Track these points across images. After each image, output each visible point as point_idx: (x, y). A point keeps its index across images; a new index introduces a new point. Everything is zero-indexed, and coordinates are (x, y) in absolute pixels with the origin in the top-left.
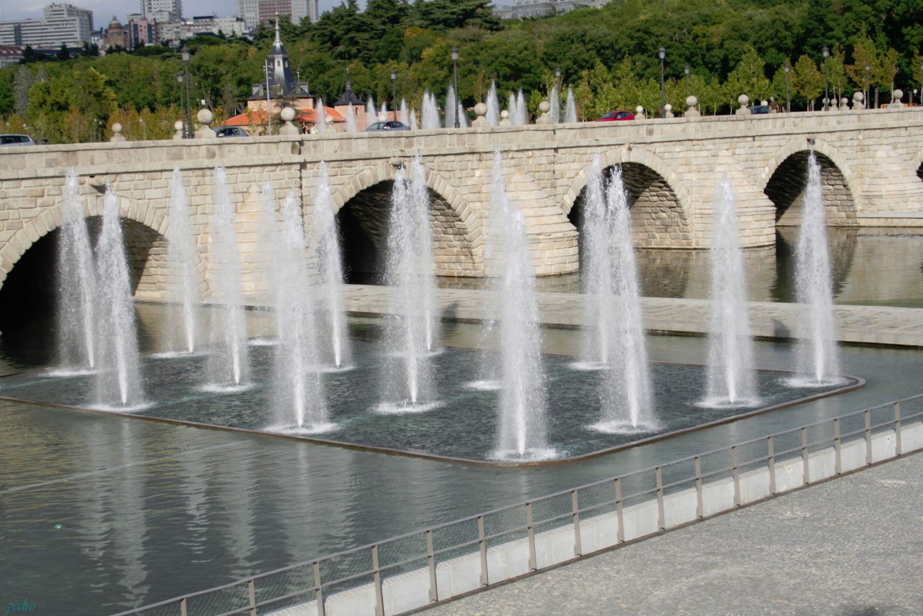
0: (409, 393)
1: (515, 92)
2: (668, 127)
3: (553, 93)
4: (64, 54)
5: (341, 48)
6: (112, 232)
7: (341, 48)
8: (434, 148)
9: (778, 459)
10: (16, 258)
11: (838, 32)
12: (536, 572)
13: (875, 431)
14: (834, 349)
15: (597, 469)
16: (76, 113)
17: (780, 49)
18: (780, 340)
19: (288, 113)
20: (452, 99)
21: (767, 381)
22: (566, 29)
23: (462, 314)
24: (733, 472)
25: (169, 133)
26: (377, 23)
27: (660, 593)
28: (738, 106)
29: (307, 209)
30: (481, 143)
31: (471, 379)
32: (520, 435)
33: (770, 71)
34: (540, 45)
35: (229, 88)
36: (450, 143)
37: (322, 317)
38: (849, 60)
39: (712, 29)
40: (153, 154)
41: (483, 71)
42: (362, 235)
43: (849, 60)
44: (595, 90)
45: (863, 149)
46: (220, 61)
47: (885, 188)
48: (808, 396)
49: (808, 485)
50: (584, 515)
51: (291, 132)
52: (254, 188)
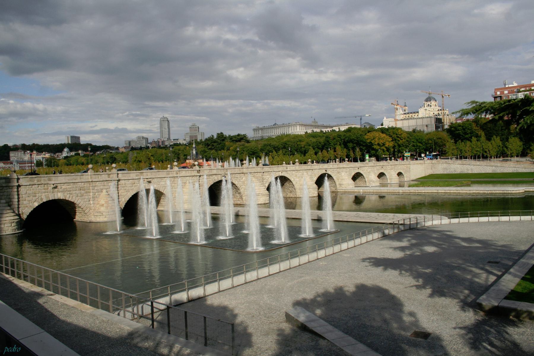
0: (226, 234)
1: (253, 158)
2: (291, 167)
3: (263, 159)
4: (141, 148)
5: (210, 147)
6: (152, 192)
7: (210, 147)
8: (233, 172)
9: (319, 250)
10: (128, 199)
11: (332, 144)
12: (259, 279)
13: (342, 242)
14: (332, 223)
15: (274, 253)
16: (143, 163)
17: (318, 148)
18: (319, 220)
19: (196, 163)
20: (237, 160)
21: (316, 230)
22: (266, 143)
23: (240, 214)
24: (307, 253)
25: (166, 168)
26: (219, 141)
27: (290, 284)
28: (308, 162)
29: (201, 187)
30: (245, 171)
31: (243, 230)
32: (255, 244)
33: (316, 154)
34: (260, 147)
35: (182, 157)
36: (237, 171)
37: (204, 213)
38: (335, 151)
39: (302, 143)
40: (162, 173)
41: (245, 153)
42: (215, 194)
43: (335, 151)
44: (273, 158)
45: (339, 173)
46: (179, 150)
47: (344, 182)
48: (326, 234)
49: (326, 256)
50: (270, 265)
51: (197, 168)
52: (188, 182)
